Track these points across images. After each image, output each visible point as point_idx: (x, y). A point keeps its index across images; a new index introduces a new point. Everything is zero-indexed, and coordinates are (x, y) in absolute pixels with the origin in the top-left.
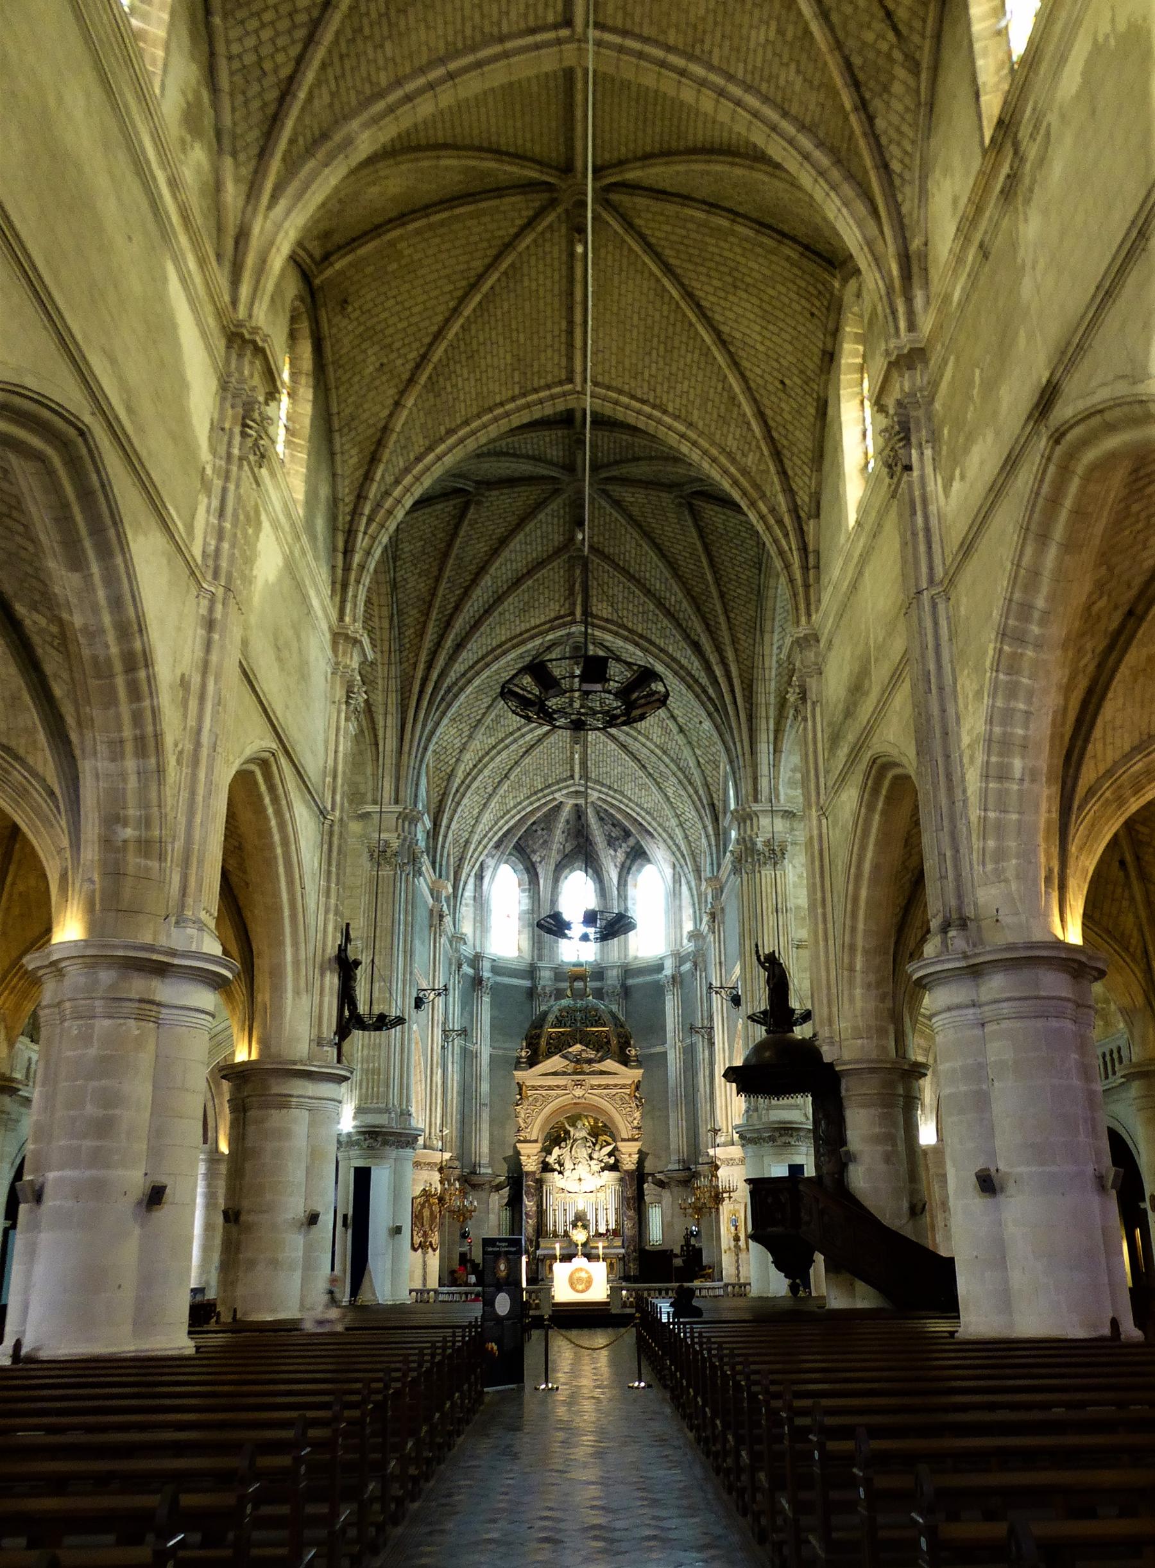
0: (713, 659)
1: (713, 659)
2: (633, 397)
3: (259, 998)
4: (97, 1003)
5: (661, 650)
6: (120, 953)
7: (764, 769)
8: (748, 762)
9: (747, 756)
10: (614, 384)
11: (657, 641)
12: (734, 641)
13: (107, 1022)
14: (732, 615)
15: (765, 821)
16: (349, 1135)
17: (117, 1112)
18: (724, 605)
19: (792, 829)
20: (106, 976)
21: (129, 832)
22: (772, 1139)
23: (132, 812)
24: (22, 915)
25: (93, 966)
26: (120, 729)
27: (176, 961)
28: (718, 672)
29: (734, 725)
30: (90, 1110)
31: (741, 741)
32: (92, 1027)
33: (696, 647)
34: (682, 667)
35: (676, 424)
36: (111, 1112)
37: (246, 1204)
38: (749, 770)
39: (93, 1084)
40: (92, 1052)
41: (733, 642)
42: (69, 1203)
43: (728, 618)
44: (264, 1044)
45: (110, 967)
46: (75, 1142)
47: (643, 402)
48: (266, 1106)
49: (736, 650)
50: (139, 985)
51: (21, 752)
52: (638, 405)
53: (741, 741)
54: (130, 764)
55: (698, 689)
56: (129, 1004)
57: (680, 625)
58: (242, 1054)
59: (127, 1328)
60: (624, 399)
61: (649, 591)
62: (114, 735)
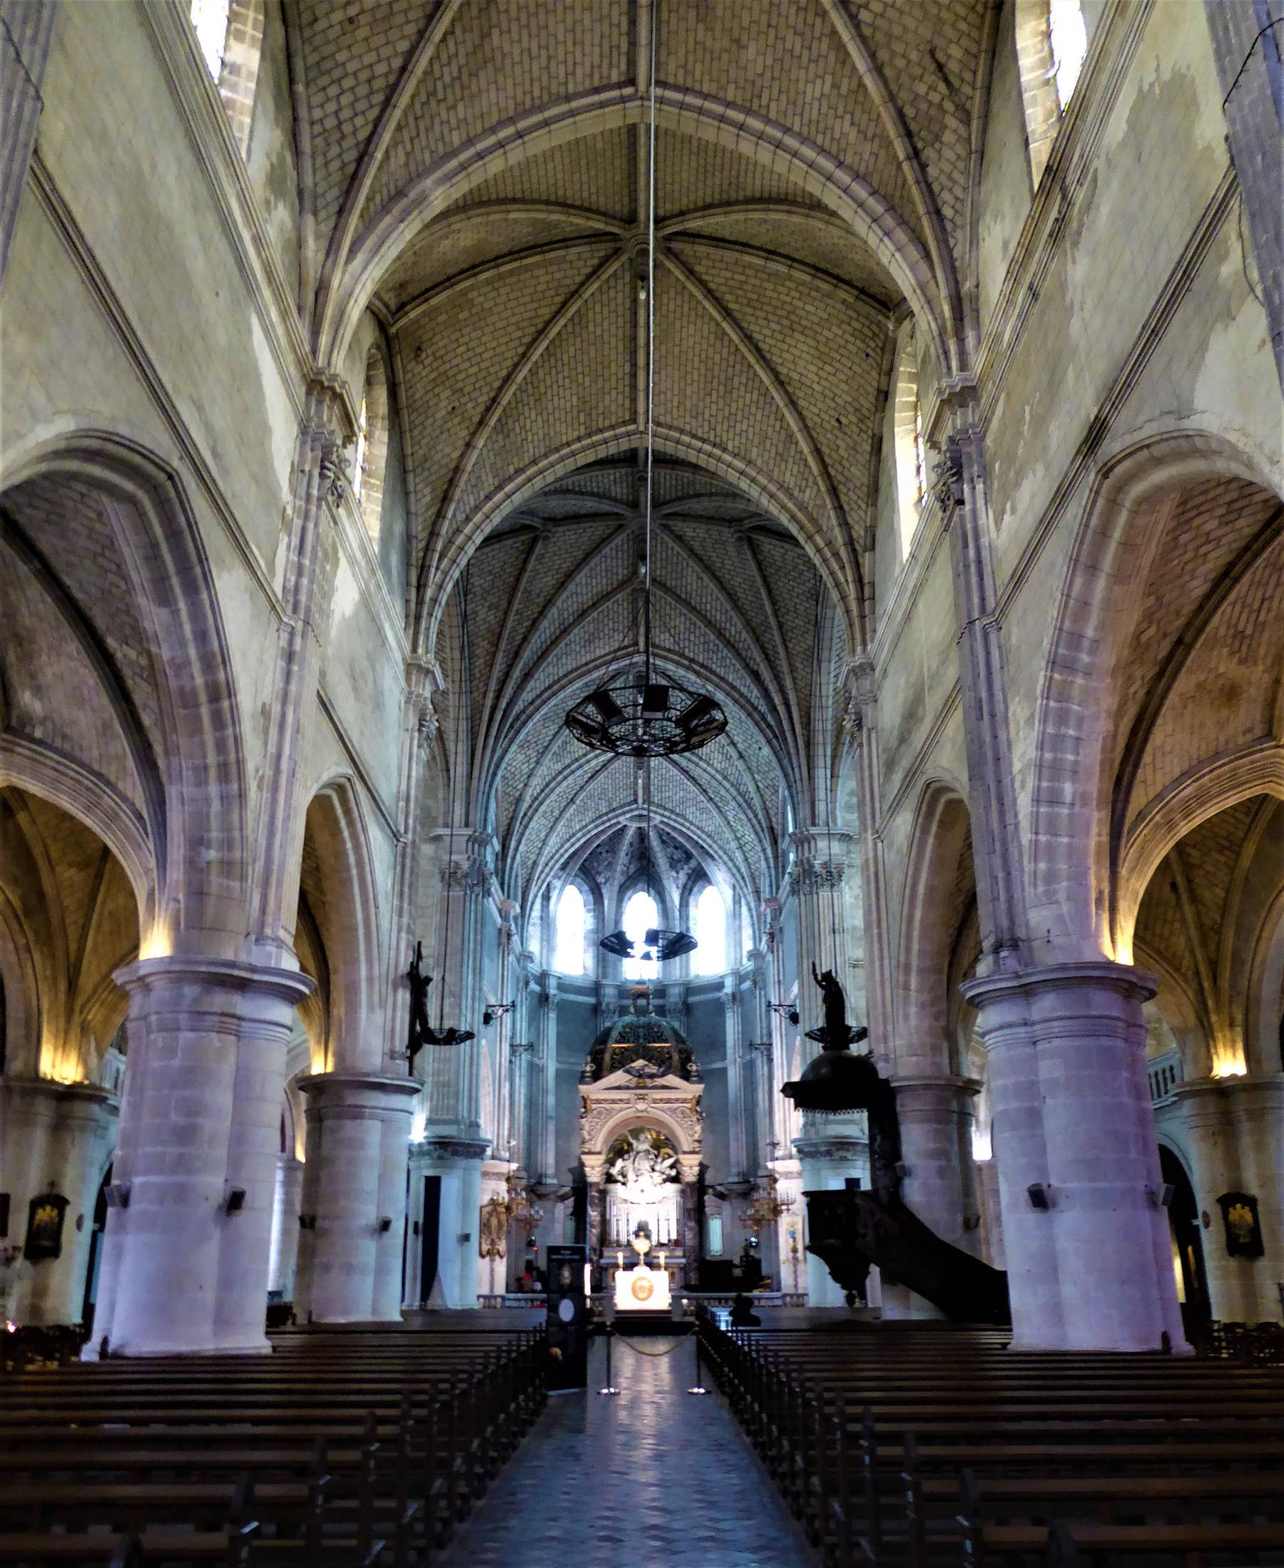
0: (772, 687)
1: (772, 687)
2: (694, 436)
5: (722, 679)
6: (203, 969)
7: (821, 793)
10: (676, 423)
12: (792, 670)
13: (190, 1035)
15: (822, 844)
16: (420, 1145)
20: (190, 991)
22: (829, 1153)
30: (176, 1118)
32: (176, 1039)
34: (742, 695)
35: (736, 463)
37: (321, 1211)
40: (176, 1063)
42: (153, 1208)
44: (340, 1058)
47: (704, 441)
48: (340, 1116)
49: (794, 679)
50: (221, 1000)
51: (112, 778)
52: (698, 444)
54: (214, 789)
58: (320, 1065)
62: (198, 762)
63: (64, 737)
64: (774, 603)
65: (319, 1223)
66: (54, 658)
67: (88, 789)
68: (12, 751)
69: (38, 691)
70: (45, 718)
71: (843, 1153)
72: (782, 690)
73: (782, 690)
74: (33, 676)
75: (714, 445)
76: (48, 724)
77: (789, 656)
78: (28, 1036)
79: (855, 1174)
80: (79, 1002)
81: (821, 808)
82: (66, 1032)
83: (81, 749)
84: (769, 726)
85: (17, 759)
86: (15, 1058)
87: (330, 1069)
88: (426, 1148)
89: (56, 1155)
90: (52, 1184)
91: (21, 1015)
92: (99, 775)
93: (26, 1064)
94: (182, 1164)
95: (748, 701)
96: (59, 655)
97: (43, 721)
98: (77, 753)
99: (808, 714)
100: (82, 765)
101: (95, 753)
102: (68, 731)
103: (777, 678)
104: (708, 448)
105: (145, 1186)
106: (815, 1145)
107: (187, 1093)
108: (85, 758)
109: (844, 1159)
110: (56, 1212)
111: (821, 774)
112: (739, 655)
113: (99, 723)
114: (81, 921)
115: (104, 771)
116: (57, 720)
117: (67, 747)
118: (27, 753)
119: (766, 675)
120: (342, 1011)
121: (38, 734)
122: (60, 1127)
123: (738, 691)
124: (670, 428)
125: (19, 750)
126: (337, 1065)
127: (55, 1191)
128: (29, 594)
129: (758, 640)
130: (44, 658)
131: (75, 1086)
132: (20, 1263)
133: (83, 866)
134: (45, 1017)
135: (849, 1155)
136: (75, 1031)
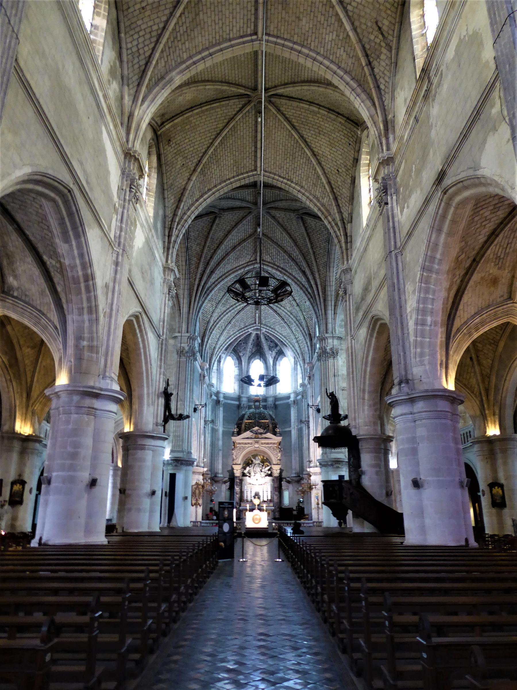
0: (310, 277)
1: (310, 277)
2: (280, 176)
5: (290, 274)
6: (81, 389)
7: (330, 320)
10: (272, 171)
13: (76, 416)
15: (330, 341)
16: (168, 461)
17: (79, 450)
18: (315, 257)
20: (76, 398)
21: (85, 343)
22: (332, 465)
26: (82, 304)
29: (318, 303)
30: (69, 449)
32: (70, 417)
34: (298, 280)
40: (70, 427)
42: (61, 485)
44: (136, 425)
46: (63, 461)
47: (284, 178)
48: (136, 449)
49: (319, 274)
50: (88, 402)
51: (45, 312)
52: (282, 179)
54: (86, 317)
58: (128, 428)
62: (80, 306)
63: (26, 295)
67: (36, 316)
68: (5, 301)
69: (15, 277)
70: (18, 288)
71: (338, 465)
72: (314, 279)
73: (314, 279)
74: (13, 271)
75: (288, 180)
76: (20, 290)
77: (317, 265)
78: (10, 416)
79: (342, 473)
80: (31, 402)
81: (330, 326)
82: (26, 414)
83: (33, 300)
84: (309, 293)
85: (7, 304)
86: (5, 424)
87: (132, 430)
89: (22, 463)
90: (20, 475)
91: (8, 407)
92: (40, 311)
93: (10, 427)
94: (72, 468)
95: (301, 283)
97: (17, 289)
98: (31, 302)
99: (325, 288)
102: (27, 293)
107: (74, 439)
108: (34, 304)
109: (338, 467)
110: (21, 486)
111: (330, 313)
112: (297, 264)
113: (40, 290)
114: (32, 370)
115: (42, 309)
117: (27, 299)
120: (137, 406)
121: (15, 294)
122: (23, 452)
123: (297, 279)
124: (270, 173)
125: (8, 300)
126: (134, 428)
127: (21, 478)
129: (305, 258)
130: (18, 264)
131: (29, 436)
133: (33, 348)
135: (340, 466)
136: (30, 414)
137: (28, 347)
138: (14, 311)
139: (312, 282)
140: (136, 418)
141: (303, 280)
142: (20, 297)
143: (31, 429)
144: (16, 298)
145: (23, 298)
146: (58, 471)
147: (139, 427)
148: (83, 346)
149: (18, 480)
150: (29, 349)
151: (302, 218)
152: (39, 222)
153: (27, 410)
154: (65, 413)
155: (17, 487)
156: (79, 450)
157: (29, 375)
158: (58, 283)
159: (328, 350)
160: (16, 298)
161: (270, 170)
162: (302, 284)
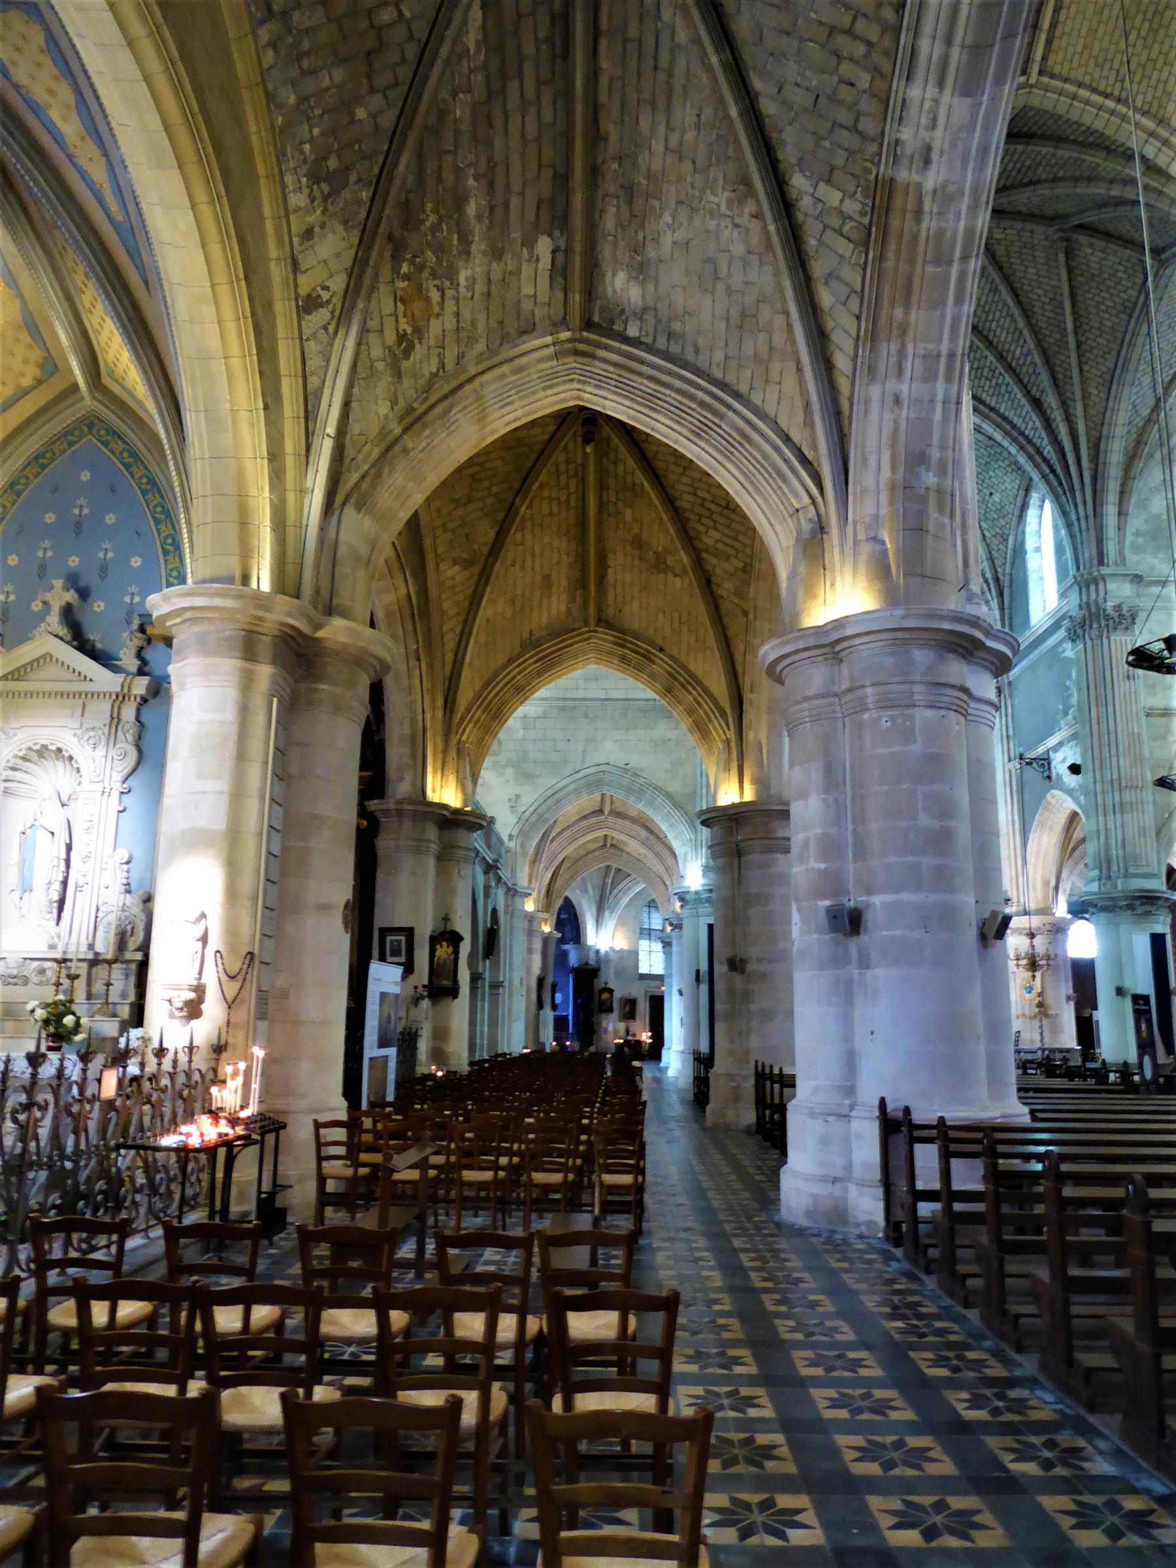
0: (1057, 415)
1: (1057, 415)
2: (1094, 90)
3: (750, 736)
4: (916, 688)
5: (992, 409)
6: (947, 626)
7: (1111, 531)
8: (1092, 525)
9: (1091, 518)
10: (1073, 75)
11: (988, 400)
12: (1085, 396)
13: (929, 713)
14: (1086, 368)
15: (1112, 586)
16: (697, 893)
17: (953, 823)
18: (1080, 356)
19: (1138, 595)
20: (922, 656)
21: (931, 479)
22: (1131, 907)
23: (935, 454)
24: (487, 644)
25: (905, 642)
26: (940, 341)
27: (990, 643)
28: (1063, 431)
29: (1077, 486)
30: (925, 820)
31: (1085, 503)
32: (911, 718)
33: (1037, 404)
34: (1014, 427)
35: (1144, 121)
36: (946, 823)
37: (753, 952)
38: (1092, 533)
39: (922, 789)
40: (916, 748)
41: (1084, 397)
42: (917, 934)
43: (1081, 371)
44: (761, 783)
45: (926, 644)
46: (910, 859)
47: (1107, 96)
48: (771, 850)
49: (1085, 406)
50: (957, 670)
51: (743, 388)
52: (1099, 99)
53: (1085, 503)
54: (940, 387)
55: (1031, 450)
56: (950, 692)
57: (1021, 381)
58: (729, 794)
59: (983, 1091)
60: (1084, 93)
61: (991, 344)
62: (931, 346)
63: (670, 335)
64: (1076, 319)
65: (751, 967)
66: (683, 217)
67: (703, 405)
68: (593, 356)
69: (641, 271)
70: (645, 310)
71: (1147, 908)
72: (1069, 420)
73: (1069, 420)
74: (637, 249)
75: (1119, 101)
76: (649, 318)
77: (1084, 381)
78: (413, 756)
79: (1159, 929)
80: (458, 717)
81: (1111, 547)
82: (445, 752)
83: (697, 351)
84: (1045, 460)
85: (598, 367)
86: (401, 779)
87: (749, 796)
88: (705, 896)
89: (445, 889)
90: (446, 919)
91: (407, 731)
92: (723, 385)
93: (413, 786)
94: (943, 879)
95: (1022, 434)
96: (694, 211)
97: (640, 315)
98: (690, 357)
99: (1098, 445)
100: (697, 372)
101: (719, 355)
102: (677, 326)
103: (1065, 405)
104: (1110, 104)
105: (886, 906)
106: (1112, 899)
107: (936, 787)
108: (702, 362)
109: (1148, 913)
110: (451, 950)
111: (1111, 510)
112: (1021, 381)
113: (735, 311)
114: (459, 629)
115: (730, 379)
116: (664, 313)
117: (675, 348)
118: (614, 357)
119: (1051, 400)
120: (763, 735)
121: (632, 331)
122: (446, 856)
123: (1010, 423)
124: (1066, 80)
125: (602, 353)
126: (758, 792)
127: (449, 928)
128: (677, 114)
129: (1047, 362)
130: (667, 218)
131: (456, 812)
132: (425, 1004)
133: (467, 564)
134: (429, 734)
135: (1153, 909)
136: (453, 753)
137: (455, 562)
138: (624, 390)
139: (1063, 431)
140: (759, 763)
141: (1032, 425)
142: (648, 340)
143: (460, 795)
144: (635, 342)
145: (661, 343)
146: (896, 890)
147: (774, 791)
148: (927, 489)
149: (443, 933)
150: (457, 568)
151: (1068, 240)
152: (832, 30)
153: (446, 742)
154: (885, 704)
155: (443, 951)
156: (953, 823)
157: (450, 643)
158: (829, 277)
159: (1110, 611)
160: (635, 342)
161: (1065, 73)
162: (1026, 438)
